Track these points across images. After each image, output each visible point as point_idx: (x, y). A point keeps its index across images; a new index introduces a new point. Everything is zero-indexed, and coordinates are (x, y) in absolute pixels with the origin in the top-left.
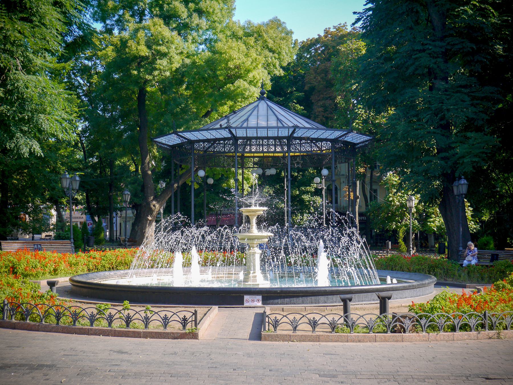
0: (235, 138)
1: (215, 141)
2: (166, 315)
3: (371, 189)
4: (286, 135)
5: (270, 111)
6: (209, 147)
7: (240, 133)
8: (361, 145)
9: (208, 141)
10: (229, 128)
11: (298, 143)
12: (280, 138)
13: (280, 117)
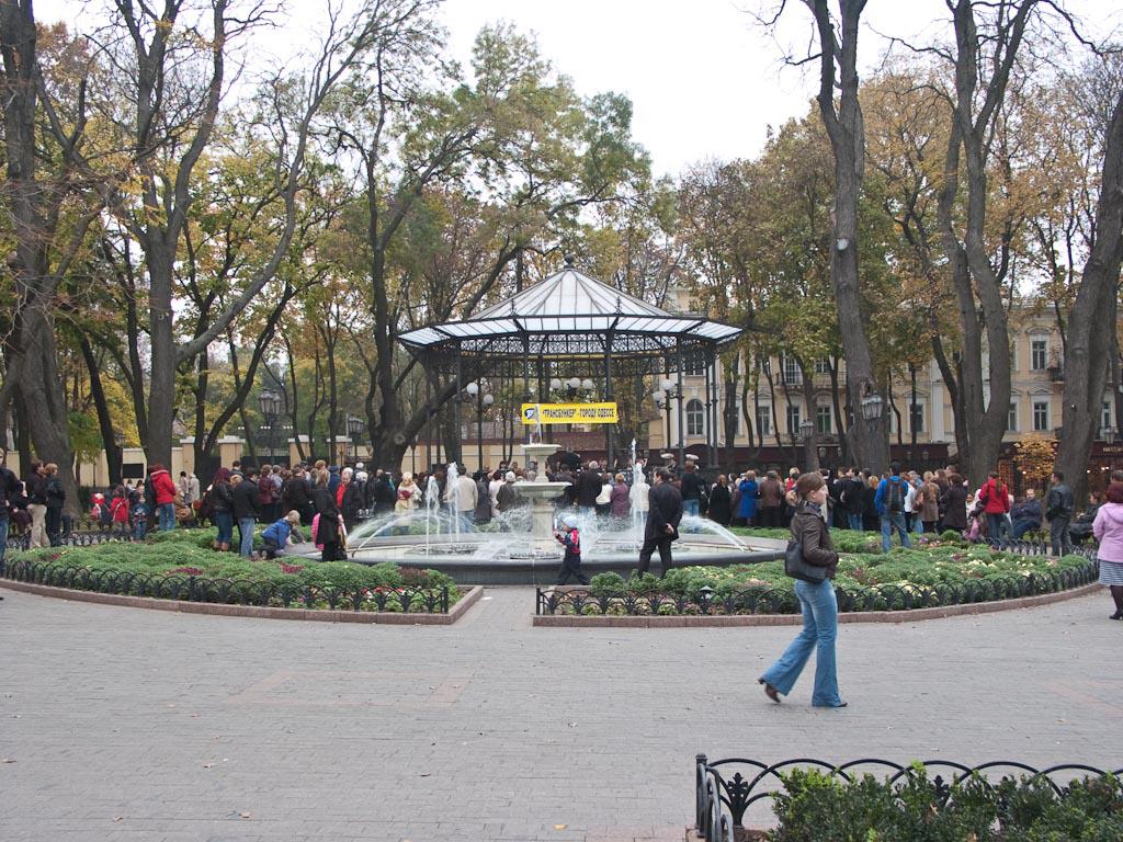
0: (523, 335)
1: (494, 337)
2: (738, 777)
3: (757, 408)
4: (605, 327)
6: (484, 347)
7: (533, 325)
8: (724, 340)
9: (483, 337)
10: (514, 317)
11: (563, 341)
12: (598, 332)
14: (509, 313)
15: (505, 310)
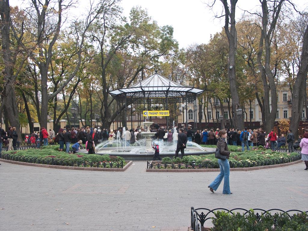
0: (143, 92)
1: (135, 92)
2: (202, 213)
4: (166, 90)
5: (159, 79)
6: (133, 95)
7: (146, 89)
8: (199, 93)
9: (132, 92)
10: (141, 87)
11: (154, 94)
12: (164, 91)
13: (163, 82)
14: (140, 86)
15: (139, 85)
